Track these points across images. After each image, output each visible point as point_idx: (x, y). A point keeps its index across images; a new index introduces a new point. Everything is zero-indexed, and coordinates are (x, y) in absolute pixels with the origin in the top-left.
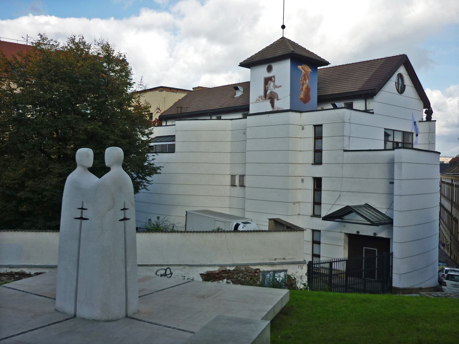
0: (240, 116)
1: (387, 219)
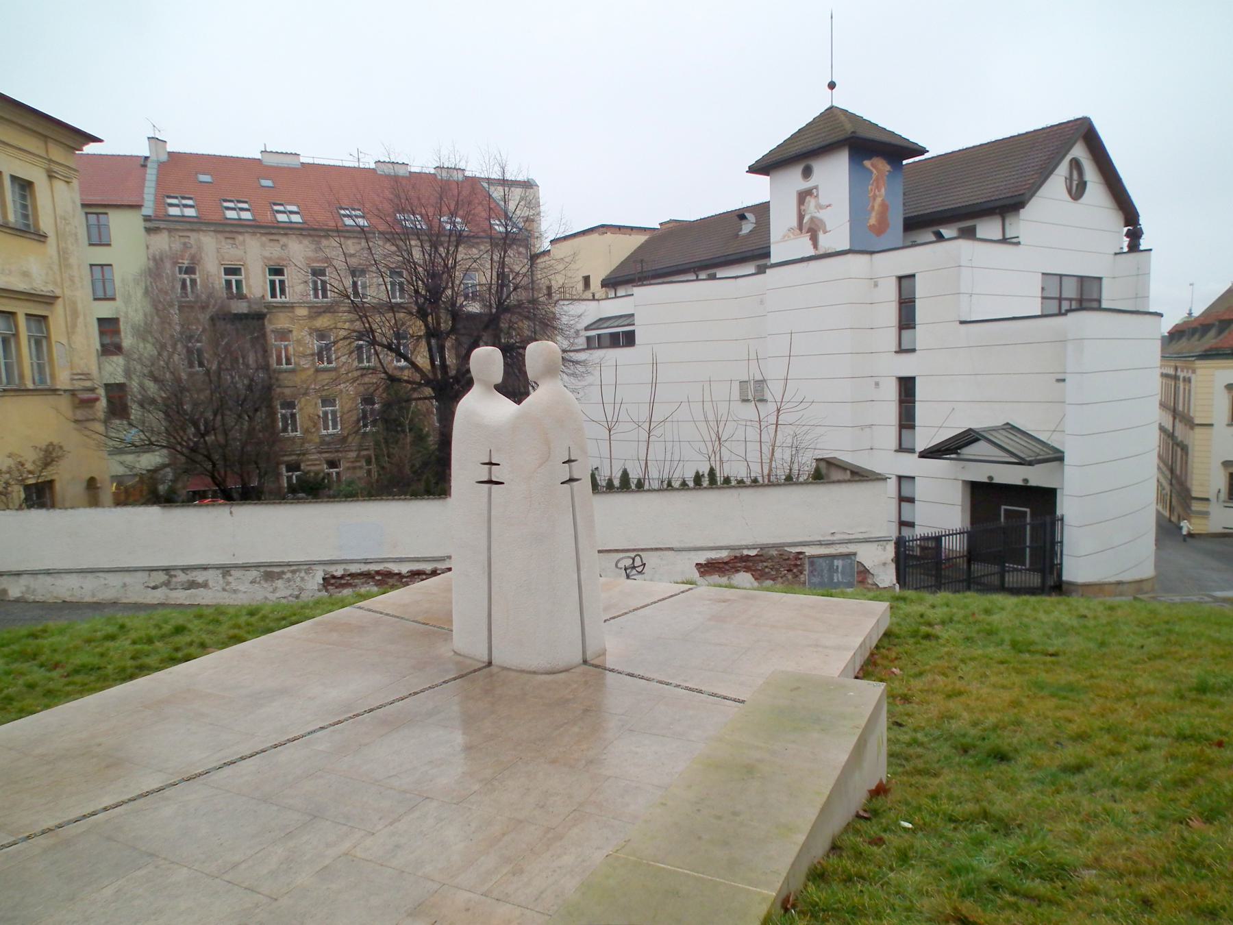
0: (750, 268)
1: (1051, 452)
